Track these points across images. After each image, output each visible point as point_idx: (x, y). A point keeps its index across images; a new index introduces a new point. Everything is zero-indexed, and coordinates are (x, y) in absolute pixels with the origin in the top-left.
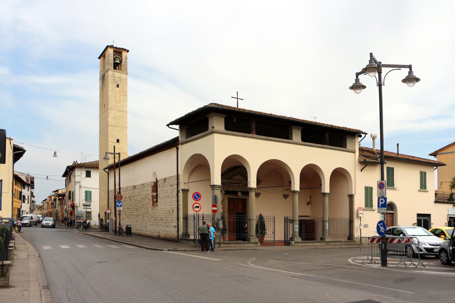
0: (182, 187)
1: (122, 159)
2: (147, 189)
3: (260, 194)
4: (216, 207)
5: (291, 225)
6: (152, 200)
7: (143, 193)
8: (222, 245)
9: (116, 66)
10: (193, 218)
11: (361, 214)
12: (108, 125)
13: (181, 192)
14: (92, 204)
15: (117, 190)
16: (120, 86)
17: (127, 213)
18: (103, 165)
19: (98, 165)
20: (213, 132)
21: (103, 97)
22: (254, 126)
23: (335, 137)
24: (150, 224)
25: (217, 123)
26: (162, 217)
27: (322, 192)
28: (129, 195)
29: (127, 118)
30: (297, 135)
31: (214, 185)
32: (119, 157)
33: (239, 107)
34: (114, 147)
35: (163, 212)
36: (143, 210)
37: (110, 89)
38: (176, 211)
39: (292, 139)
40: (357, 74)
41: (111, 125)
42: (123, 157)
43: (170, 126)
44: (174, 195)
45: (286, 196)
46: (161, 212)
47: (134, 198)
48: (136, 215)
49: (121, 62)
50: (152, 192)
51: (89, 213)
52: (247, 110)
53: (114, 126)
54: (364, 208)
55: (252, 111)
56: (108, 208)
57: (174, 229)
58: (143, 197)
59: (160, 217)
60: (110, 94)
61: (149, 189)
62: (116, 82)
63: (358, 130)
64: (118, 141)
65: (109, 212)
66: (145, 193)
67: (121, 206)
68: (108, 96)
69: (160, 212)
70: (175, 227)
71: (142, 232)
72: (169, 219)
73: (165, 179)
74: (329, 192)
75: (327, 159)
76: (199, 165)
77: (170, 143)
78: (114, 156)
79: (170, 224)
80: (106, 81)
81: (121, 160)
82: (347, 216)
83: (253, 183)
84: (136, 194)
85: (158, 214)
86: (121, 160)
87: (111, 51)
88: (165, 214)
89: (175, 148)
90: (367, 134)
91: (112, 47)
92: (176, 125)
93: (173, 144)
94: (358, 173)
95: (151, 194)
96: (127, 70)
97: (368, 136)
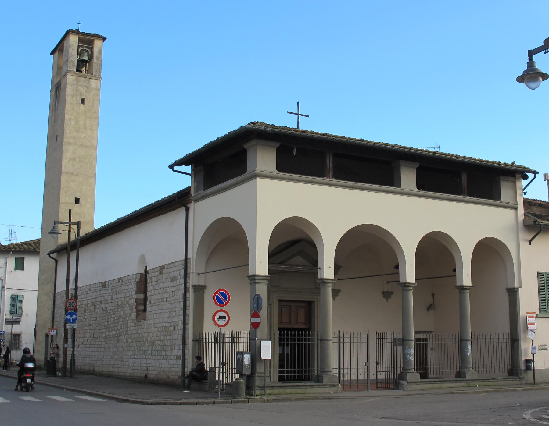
0: (193, 280)
1: (83, 233)
2: (127, 288)
3: (205, 287)
4: (258, 316)
5: (399, 349)
6: (137, 307)
7: (119, 296)
8: (268, 391)
9: (81, 64)
10: (213, 340)
11: (533, 324)
12: (60, 173)
13: (191, 290)
14: (23, 319)
15: (72, 292)
16: (86, 101)
17: (87, 335)
18: (45, 249)
19: (39, 248)
20: (255, 176)
21: (55, 122)
22: (329, 164)
23: (481, 180)
24: (131, 353)
25: (264, 159)
26: (153, 339)
27: (458, 284)
28: (93, 300)
29: (95, 159)
30: (408, 178)
31: (254, 276)
32: (79, 229)
33: (300, 129)
34: (70, 210)
35: (156, 330)
36: (119, 327)
37: (68, 106)
38: (181, 327)
39: (399, 186)
40: (531, 53)
41: (67, 173)
42: (85, 231)
43: (176, 168)
44: (178, 297)
45: (387, 295)
46: (153, 330)
47: (103, 306)
48: (105, 338)
49: (91, 57)
50: (137, 293)
51: (17, 337)
52: (317, 133)
53: (72, 174)
54: (538, 313)
55: (328, 135)
56: (53, 326)
57: (175, 361)
58: (120, 303)
59: (149, 339)
60: (67, 117)
61: (130, 287)
62: (81, 95)
63: (521, 167)
64: (77, 201)
65: (53, 333)
66: (122, 295)
67: (74, 321)
68: (63, 119)
69: (149, 331)
70: (178, 358)
71: (115, 370)
72: (168, 343)
73: (162, 268)
74: (470, 284)
75: (467, 222)
76: (228, 239)
77: (175, 200)
78: (70, 228)
79: (169, 353)
80: (62, 94)
81: (81, 235)
82: (506, 329)
83: (327, 270)
84: (106, 298)
85: (145, 335)
86: (81, 235)
87: (73, 40)
88: (159, 334)
89: (184, 208)
90: (538, 173)
91: (76, 32)
92: (187, 165)
93: (179, 201)
94: (524, 245)
95: (135, 296)
96: (100, 72)
97: (540, 177)
